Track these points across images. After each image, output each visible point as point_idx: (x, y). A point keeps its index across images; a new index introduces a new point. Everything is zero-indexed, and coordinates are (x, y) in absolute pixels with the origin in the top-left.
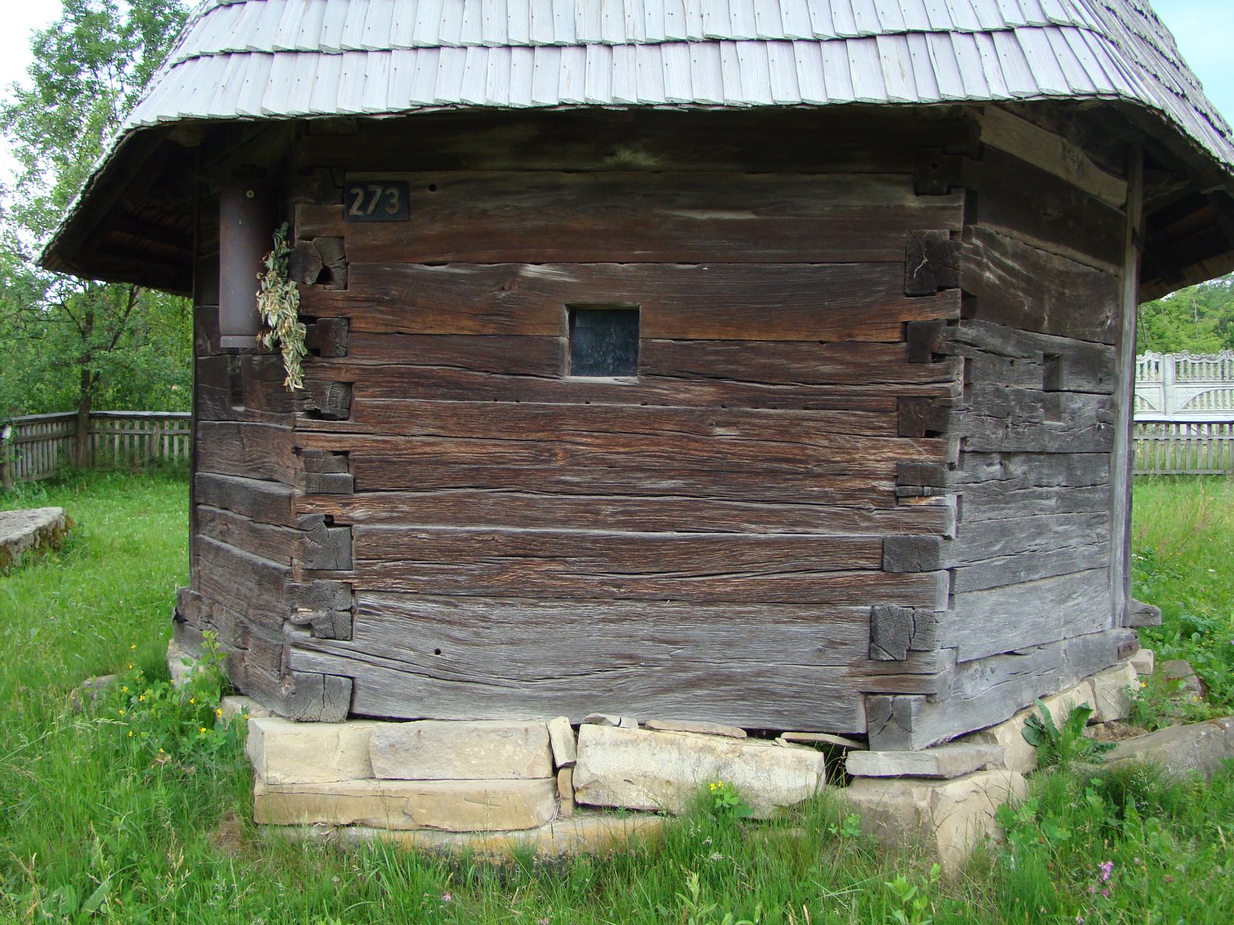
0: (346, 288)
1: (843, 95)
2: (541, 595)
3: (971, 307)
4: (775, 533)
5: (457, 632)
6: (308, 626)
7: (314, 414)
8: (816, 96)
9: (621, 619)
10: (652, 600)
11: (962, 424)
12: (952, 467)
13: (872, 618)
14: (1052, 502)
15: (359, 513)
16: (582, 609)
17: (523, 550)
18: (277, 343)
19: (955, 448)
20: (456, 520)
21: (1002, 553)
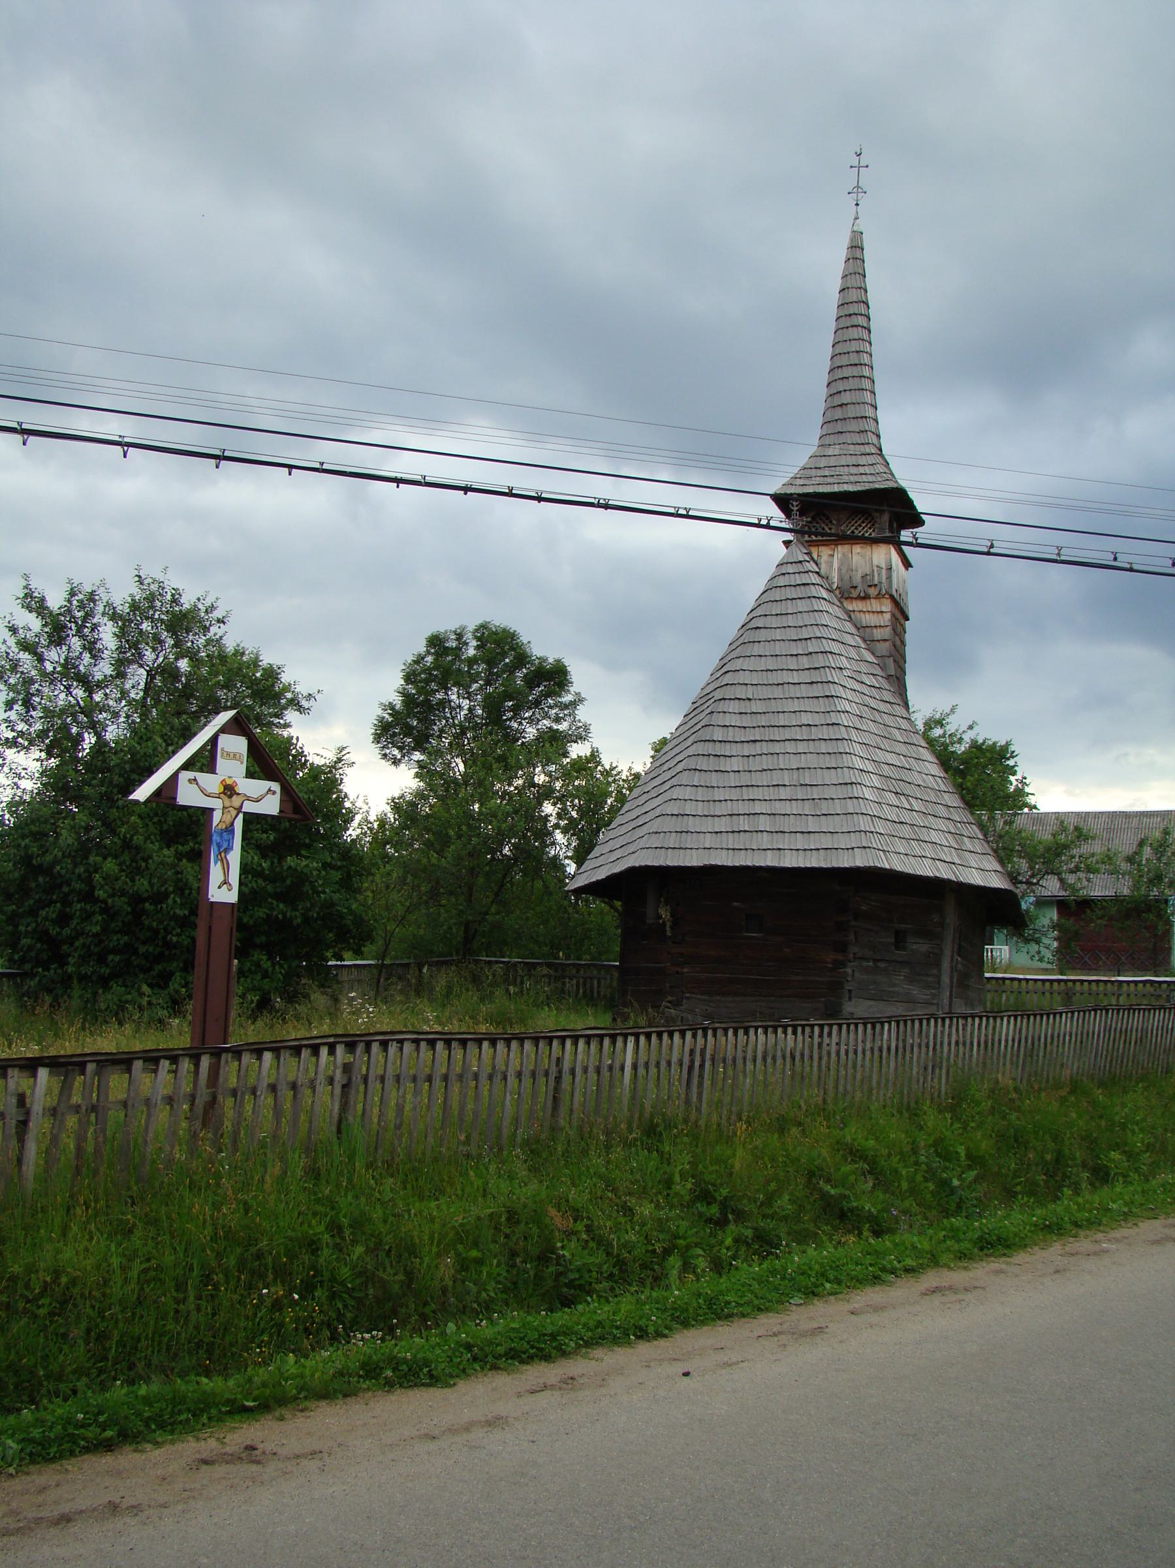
0: (992, 949)
1: (809, 865)
4: (800, 978)
11: (854, 949)
14: (902, 978)
15: (685, 970)
18: (664, 922)
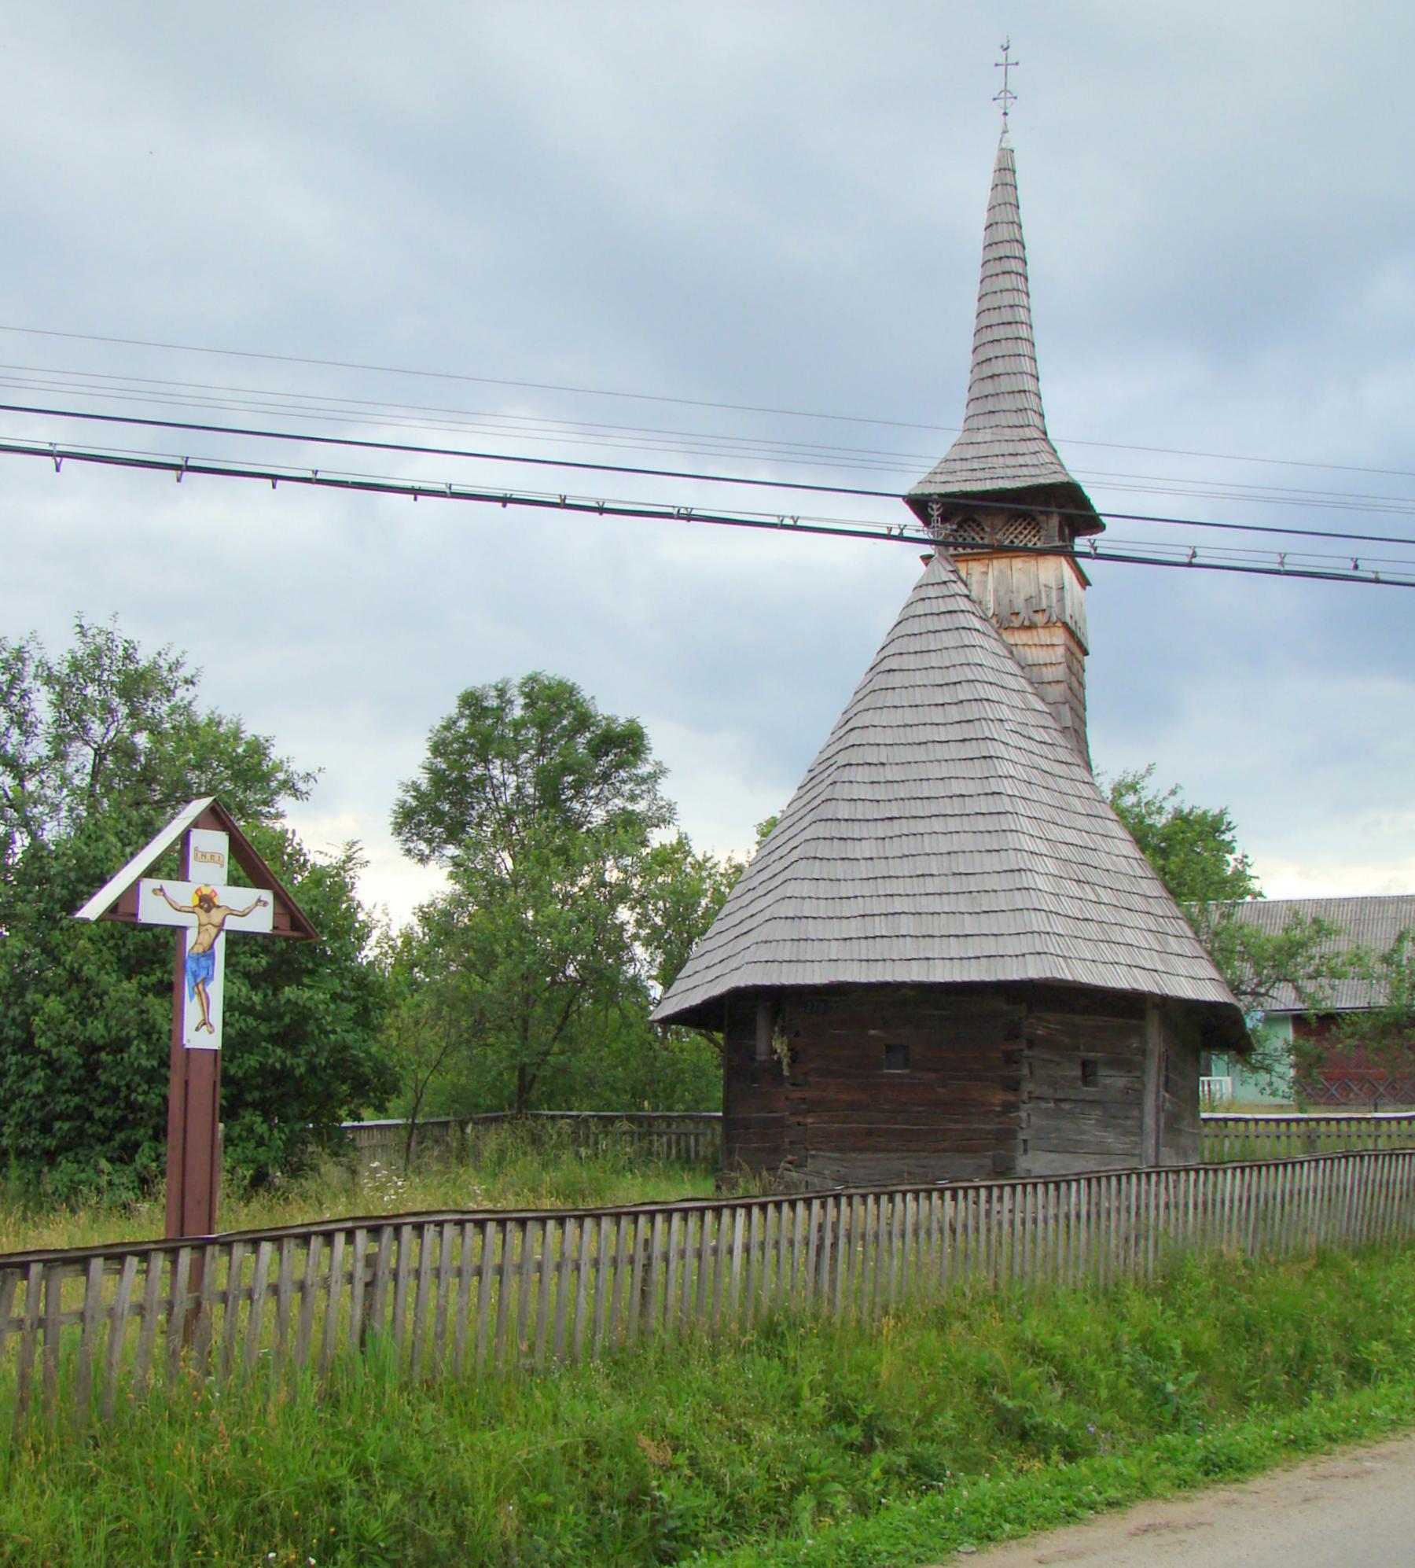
1: (966, 979)
2: (876, 1150)
3: (1031, 1044)
5: (845, 1164)
6: (790, 1163)
7: (793, 1084)
8: (958, 978)
9: (904, 1158)
10: (914, 1151)
11: (1028, 1087)
12: (1024, 1102)
13: (994, 1156)
14: (1093, 1122)
15: (809, 1120)
16: (892, 1155)
17: (869, 1133)
18: (779, 1058)
19: (1025, 1096)
20: (844, 1123)
21: (1056, 1138)
